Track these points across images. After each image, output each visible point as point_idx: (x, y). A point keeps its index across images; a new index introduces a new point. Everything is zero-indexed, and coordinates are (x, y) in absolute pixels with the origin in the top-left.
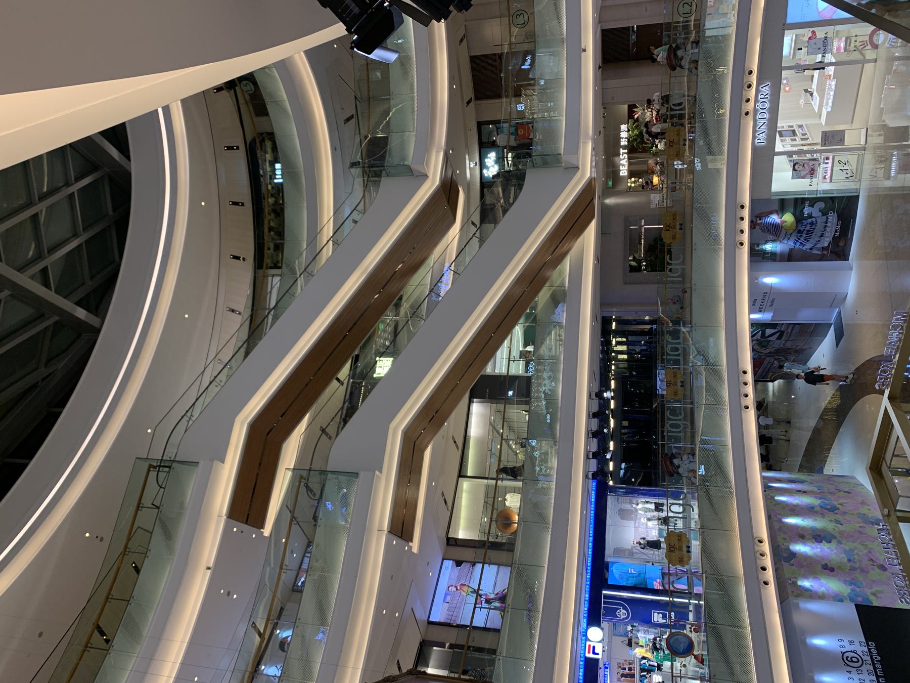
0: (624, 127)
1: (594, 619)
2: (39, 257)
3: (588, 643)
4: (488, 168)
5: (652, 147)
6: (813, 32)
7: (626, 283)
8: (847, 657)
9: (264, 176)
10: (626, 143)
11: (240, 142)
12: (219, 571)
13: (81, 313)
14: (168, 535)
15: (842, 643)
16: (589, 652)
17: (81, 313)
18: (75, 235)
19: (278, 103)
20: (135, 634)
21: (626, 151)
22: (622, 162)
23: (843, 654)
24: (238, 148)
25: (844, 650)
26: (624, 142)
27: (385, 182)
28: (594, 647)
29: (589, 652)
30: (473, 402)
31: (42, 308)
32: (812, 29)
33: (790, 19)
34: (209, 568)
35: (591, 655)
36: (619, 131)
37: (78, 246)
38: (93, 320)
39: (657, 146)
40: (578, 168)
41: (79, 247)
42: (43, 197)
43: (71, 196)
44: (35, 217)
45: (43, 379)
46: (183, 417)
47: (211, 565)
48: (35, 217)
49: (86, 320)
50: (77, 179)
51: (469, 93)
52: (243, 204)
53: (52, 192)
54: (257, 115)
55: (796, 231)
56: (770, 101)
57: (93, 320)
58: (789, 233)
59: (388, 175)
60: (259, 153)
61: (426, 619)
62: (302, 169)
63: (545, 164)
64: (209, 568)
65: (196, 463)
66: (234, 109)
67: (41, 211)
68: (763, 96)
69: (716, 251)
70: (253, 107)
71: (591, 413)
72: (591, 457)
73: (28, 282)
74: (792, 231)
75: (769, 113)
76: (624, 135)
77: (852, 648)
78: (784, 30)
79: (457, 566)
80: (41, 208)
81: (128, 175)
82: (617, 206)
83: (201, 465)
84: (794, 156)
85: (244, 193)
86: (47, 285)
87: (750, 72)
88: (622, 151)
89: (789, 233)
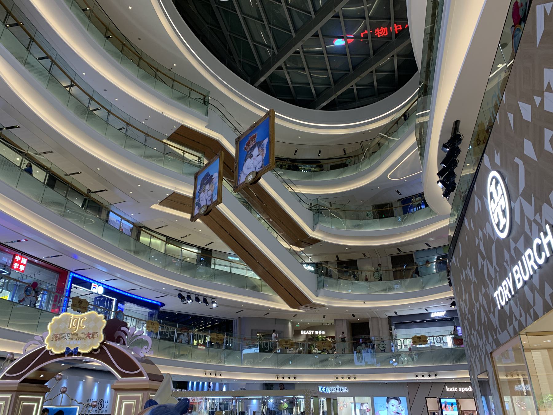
0: (323, 332)
1: (108, 291)
2: (287, 67)
3: (97, 286)
4: (307, 266)
5: (314, 347)
6: (370, 410)
7: (252, 330)
8: (102, 402)
9: (305, 166)
10: (316, 334)
11: (322, 157)
12: (161, 116)
13: (262, 79)
14: (179, 99)
15: (107, 402)
16: (94, 285)
17: (262, 79)
18: (292, 83)
19: (341, 173)
20: (143, 78)
21: (313, 334)
22: (307, 331)
23: (103, 400)
24: (319, 156)
25: (104, 401)
26: (317, 332)
27: (311, 213)
28: (95, 288)
29: (94, 285)
30: (198, 250)
31: (267, 65)
32: (371, 409)
33: (374, 398)
34: (162, 113)
35: (93, 286)
36: (322, 330)
37: (288, 82)
38: (258, 84)
39: (314, 349)
40: (317, 296)
41: (287, 83)
42: (310, 73)
43: (309, 84)
44: (303, 69)
45: (233, 58)
46: (222, 113)
47: (163, 114)
48: (303, 69)
49: (259, 81)
50: (314, 88)
51: (342, 258)
52: (295, 155)
53: (311, 76)
54: (331, 166)
55: (279, 411)
56: (340, 393)
57: (258, 84)
58: (278, 407)
59: (314, 215)
60: (315, 165)
61: (111, 209)
62: (313, 180)
63: (319, 282)
64: (162, 113)
65: (207, 115)
66: (329, 157)
67: (305, 72)
68: (342, 389)
69: (275, 365)
70: (339, 164)
71: (206, 298)
72: (188, 294)
73: (281, 63)
74: (279, 408)
75: (335, 393)
76: (320, 332)
77: (105, 406)
78: (371, 396)
79: (130, 229)
80: (307, 73)
81: (313, 108)
82: (288, 328)
83: (206, 117)
84: (498, 66)
85: (299, 156)
86: (278, 69)
87: (355, 378)
88: (313, 331)
89: (278, 407)
